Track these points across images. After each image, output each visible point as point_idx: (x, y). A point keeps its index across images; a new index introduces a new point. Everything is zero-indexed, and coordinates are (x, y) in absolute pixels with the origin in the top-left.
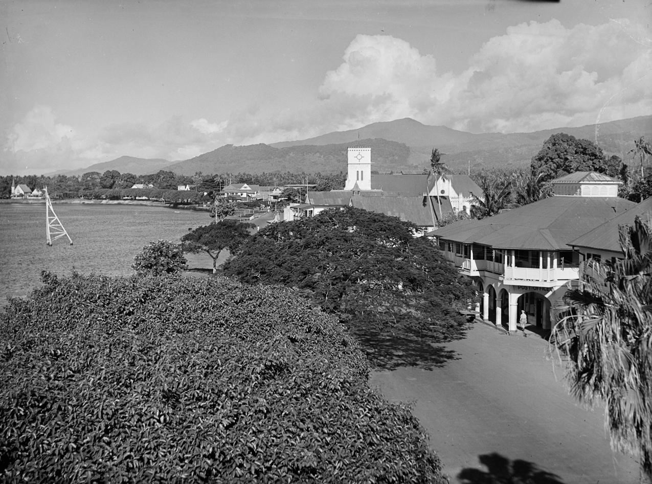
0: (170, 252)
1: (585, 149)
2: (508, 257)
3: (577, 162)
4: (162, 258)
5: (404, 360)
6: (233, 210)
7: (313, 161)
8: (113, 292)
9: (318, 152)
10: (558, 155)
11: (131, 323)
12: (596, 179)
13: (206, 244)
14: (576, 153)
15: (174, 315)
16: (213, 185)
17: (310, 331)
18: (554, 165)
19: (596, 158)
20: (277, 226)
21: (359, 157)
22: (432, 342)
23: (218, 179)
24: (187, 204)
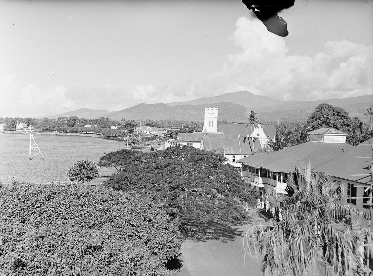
0: (89, 167)
1: (339, 113)
2: (279, 178)
3: (334, 120)
4: (84, 170)
5: (212, 236)
6: (138, 142)
7: (191, 114)
8: (31, 194)
9: (194, 109)
10: (323, 116)
11: (38, 212)
12: (333, 132)
13: (114, 162)
14: (334, 115)
15: (64, 208)
16: (130, 126)
17: (145, 220)
18: (321, 121)
19: (345, 118)
20: (142, 155)
21: (211, 113)
22: (232, 225)
23: (133, 123)
24: (115, 137)
